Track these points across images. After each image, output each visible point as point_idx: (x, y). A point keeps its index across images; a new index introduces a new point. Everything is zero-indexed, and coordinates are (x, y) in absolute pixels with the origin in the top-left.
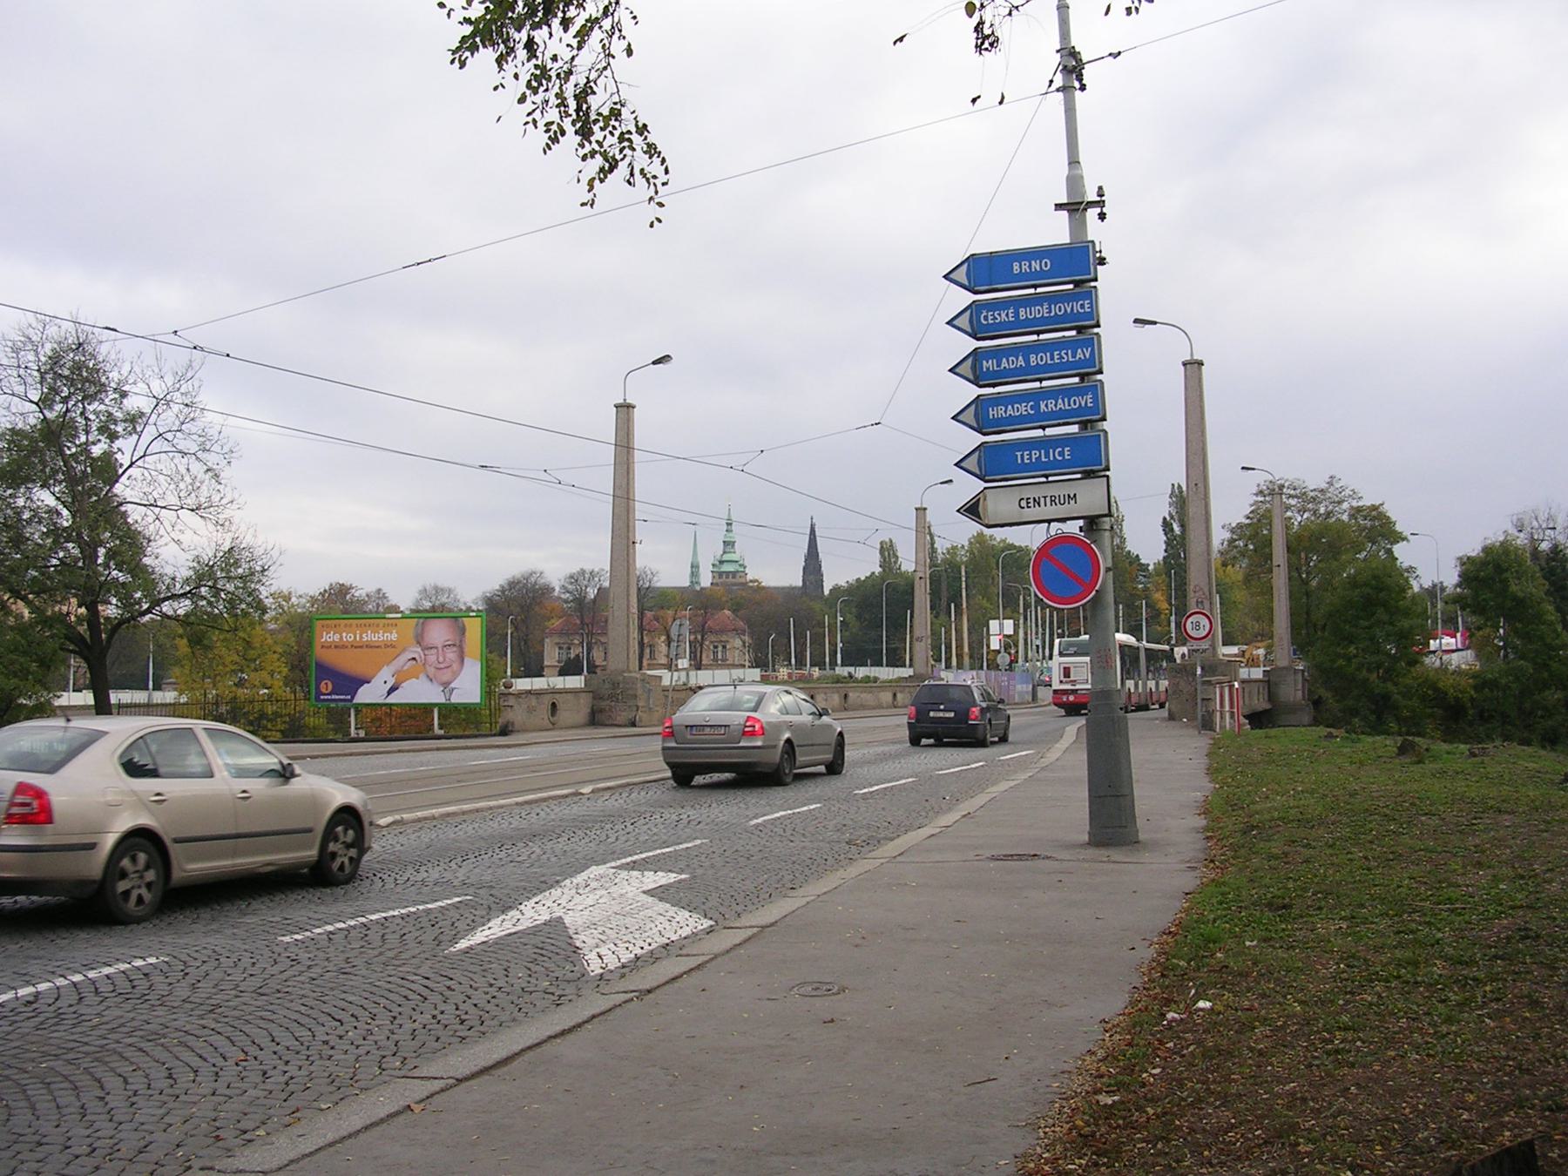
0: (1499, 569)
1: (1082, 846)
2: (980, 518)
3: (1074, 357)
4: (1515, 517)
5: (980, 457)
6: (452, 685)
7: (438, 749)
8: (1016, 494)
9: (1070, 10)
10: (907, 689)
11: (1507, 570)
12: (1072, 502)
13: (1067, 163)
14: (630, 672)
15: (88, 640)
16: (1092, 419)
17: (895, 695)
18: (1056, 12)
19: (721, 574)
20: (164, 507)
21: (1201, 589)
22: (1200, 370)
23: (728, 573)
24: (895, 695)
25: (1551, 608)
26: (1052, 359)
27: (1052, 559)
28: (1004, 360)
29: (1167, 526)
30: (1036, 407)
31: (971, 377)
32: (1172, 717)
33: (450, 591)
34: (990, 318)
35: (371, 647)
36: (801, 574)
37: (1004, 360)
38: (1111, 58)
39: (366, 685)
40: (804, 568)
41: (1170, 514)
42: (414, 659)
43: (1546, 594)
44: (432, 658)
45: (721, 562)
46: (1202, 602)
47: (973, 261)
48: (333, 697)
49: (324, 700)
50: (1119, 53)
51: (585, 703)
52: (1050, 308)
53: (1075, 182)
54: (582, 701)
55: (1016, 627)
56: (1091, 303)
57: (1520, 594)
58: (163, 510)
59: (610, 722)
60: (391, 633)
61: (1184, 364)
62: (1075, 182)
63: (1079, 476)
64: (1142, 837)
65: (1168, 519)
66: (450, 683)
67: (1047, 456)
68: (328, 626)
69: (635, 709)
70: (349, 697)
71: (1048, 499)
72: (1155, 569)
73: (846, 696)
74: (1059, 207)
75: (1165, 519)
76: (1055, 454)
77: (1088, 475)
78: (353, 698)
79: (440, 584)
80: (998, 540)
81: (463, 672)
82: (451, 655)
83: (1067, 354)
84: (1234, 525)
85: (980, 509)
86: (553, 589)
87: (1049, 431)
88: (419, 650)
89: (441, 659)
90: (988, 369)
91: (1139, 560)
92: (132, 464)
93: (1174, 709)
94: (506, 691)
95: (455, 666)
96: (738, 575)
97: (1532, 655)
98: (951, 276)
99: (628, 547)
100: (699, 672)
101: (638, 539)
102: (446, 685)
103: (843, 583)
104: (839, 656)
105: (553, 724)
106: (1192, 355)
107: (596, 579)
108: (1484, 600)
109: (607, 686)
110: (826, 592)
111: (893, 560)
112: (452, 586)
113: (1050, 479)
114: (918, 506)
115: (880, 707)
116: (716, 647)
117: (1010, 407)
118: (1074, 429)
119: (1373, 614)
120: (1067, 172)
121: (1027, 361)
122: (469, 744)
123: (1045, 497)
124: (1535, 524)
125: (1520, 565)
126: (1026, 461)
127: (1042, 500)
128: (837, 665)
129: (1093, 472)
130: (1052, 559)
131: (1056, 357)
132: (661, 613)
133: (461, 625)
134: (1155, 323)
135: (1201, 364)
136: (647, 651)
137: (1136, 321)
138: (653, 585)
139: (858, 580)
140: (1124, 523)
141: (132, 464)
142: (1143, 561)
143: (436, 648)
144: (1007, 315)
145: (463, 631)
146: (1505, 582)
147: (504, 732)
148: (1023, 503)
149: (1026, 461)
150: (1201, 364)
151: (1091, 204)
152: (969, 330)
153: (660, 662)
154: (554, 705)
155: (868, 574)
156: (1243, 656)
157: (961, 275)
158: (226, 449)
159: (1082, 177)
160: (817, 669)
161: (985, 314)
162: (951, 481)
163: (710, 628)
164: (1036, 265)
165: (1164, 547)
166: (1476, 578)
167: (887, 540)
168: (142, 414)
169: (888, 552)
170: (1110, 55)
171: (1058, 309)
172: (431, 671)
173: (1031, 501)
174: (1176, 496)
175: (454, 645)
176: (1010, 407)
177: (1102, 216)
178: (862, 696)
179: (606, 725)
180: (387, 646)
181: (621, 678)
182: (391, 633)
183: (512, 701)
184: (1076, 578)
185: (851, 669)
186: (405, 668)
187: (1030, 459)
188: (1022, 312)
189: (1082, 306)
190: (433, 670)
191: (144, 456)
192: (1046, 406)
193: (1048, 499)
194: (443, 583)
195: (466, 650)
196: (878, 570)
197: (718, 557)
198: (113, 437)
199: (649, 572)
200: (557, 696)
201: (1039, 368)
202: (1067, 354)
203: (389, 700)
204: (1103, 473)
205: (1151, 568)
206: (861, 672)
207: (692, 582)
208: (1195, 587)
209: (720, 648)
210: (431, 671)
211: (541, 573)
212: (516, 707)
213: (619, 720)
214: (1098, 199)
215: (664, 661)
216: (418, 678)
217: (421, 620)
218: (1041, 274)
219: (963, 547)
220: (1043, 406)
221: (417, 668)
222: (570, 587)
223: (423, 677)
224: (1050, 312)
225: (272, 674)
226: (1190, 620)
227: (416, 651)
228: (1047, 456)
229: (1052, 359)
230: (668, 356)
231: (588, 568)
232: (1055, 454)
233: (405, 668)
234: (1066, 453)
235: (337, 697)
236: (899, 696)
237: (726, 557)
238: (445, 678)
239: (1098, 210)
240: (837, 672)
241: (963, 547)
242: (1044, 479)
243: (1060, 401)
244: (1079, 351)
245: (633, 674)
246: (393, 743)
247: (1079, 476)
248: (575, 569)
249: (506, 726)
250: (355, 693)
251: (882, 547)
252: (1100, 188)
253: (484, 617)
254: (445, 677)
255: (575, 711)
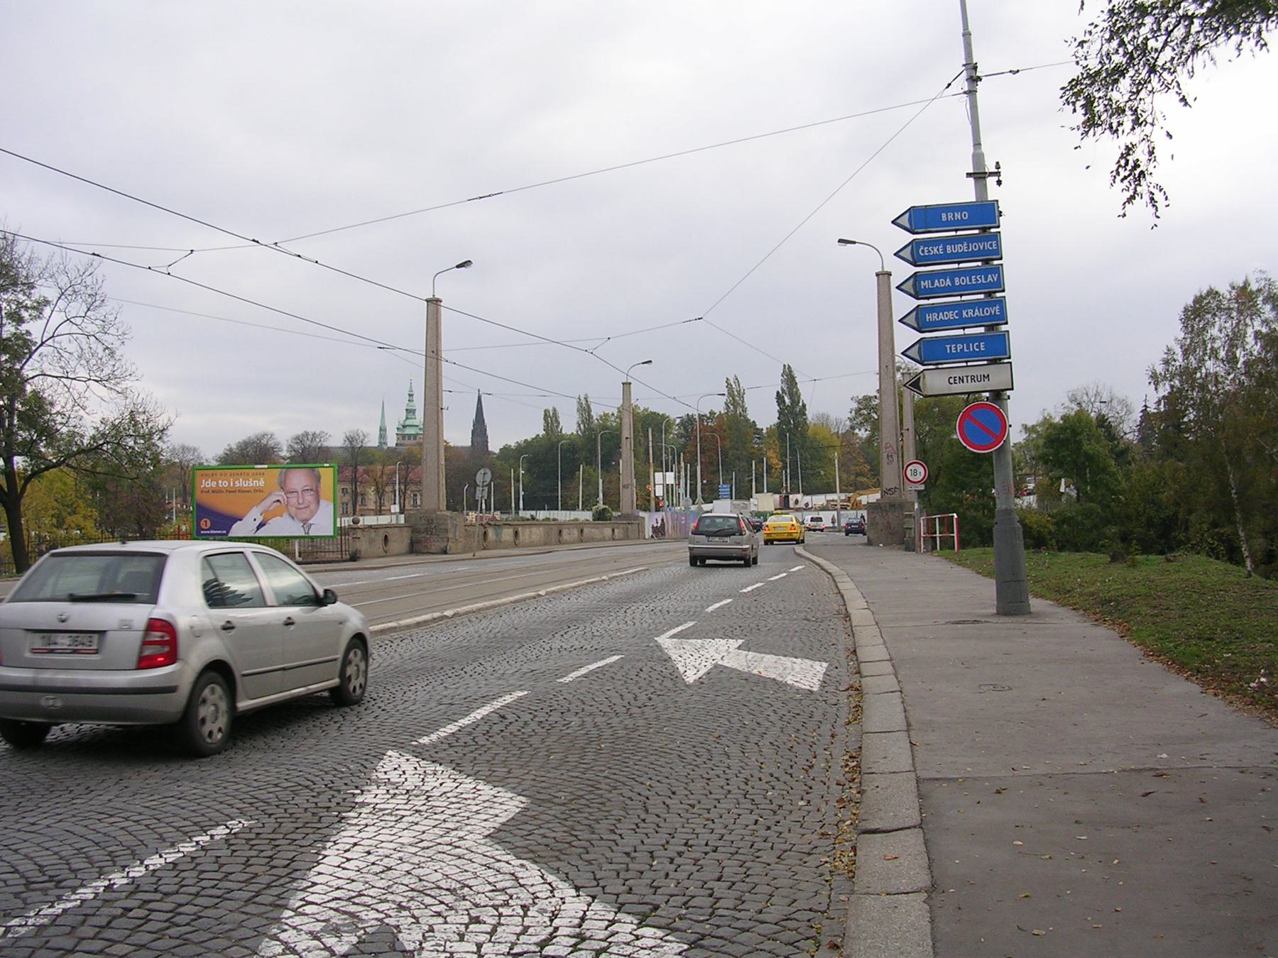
0: (1075, 433)
1: (993, 615)
2: (920, 390)
3: (986, 279)
4: (1071, 393)
5: (920, 348)
6: (310, 522)
7: (326, 571)
8: (946, 375)
9: (972, 37)
10: (621, 526)
11: (1080, 434)
12: (986, 380)
13: (972, 144)
14: (441, 511)
15: (6, 490)
16: (996, 319)
17: (613, 530)
18: (962, 38)
19: (404, 436)
20: (74, 379)
21: (891, 446)
22: (889, 279)
23: (410, 436)
24: (613, 530)
25: (1113, 463)
26: (971, 281)
27: (972, 419)
28: (936, 281)
29: (780, 398)
30: (960, 314)
31: (913, 292)
32: (870, 543)
33: (195, 450)
34: (926, 251)
35: (243, 492)
36: (471, 436)
37: (936, 281)
38: (1011, 74)
39: (239, 522)
40: (473, 432)
41: (782, 389)
42: (278, 501)
43: (1109, 452)
44: (293, 500)
45: (404, 426)
46: (891, 456)
47: (912, 211)
48: (212, 532)
49: (204, 534)
50: (1018, 71)
51: (406, 535)
52: (968, 246)
53: (978, 158)
54: (404, 534)
55: (678, 478)
56: (997, 243)
57: (1091, 452)
58: (74, 381)
59: (426, 550)
60: (259, 480)
61: (877, 275)
62: (978, 158)
63: (985, 362)
64: (1032, 609)
65: (781, 392)
66: (307, 520)
67: (968, 348)
68: (206, 475)
69: (446, 540)
70: (225, 532)
71: (969, 378)
72: (767, 432)
73: (582, 531)
74: (969, 175)
75: (778, 393)
76: (974, 347)
77: (993, 362)
78: (228, 532)
79: (186, 445)
80: (642, 409)
81: (319, 511)
82: (309, 497)
83: (981, 278)
84: (860, 397)
85: (921, 384)
86: (281, 450)
87: (968, 331)
88: (283, 493)
89: (301, 501)
90: (925, 287)
91: (755, 425)
92: (43, 343)
93: (871, 537)
94: (355, 526)
95: (313, 506)
96: (418, 437)
97: (1100, 498)
98: (898, 221)
99: (438, 412)
100: (379, 517)
101: (444, 406)
102: (305, 521)
103: (513, 444)
104: (521, 502)
105: (386, 552)
106: (883, 267)
107: (318, 440)
108: (1063, 456)
109: (423, 522)
110: (1016, 436)
111: (555, 424)
112: (195, 446)
113: (969, 364)
114: (625, 381)
115: (604, 539)
116: (415, 495)
117: (941, 314)
118: (982, 330)
119: (980, 466)
120: (972, 152)
121: (953, 282)
122: (347, 567)
123: (967, 377)
124: (1085, 398)
125: (1090, 431)
126: (953, 351)
127: (965, 378)
128: (519, 509)
129: (1000, 359)
130: (972, 419)
131: (973, 280)
132: (371, 467)
133: (316, 473)
134: (854, 243)
135: (890, 274)
136: (359, 499)
137: (840, 241)
138: (364, 445)
139: (526, 440)
140: (745, 396)
141: (43, 343)
142: (758, 427)
143: (297, 492)
144: (938, 250)
145: (318, 478)
146: (1079, 443)
147: (354, 558)
148: (952, 381)
149: (953, 351)
150: (890, 274)
151: (991, 174)
152: (910, 259)
153: (370, 507)
154: (386, 537)
155: (534, 436)
156: (849, 501)
157: (905, 221)
158: (120, 332)
159: (983, 154)
160: (499, 513)
161: (922, 248)
162: (651, 361)
163: (411, 480)
164: (958, 216)
165: (777, 415)
166: (1057, 440)
167: (551, 409)
168: (47, 302)
169: (551, 419)
170: (1011, 71)
171: (973, 247)
172: (293, 510)
173: (957, 379)
174: (787, 375)
175: (311, 490)
176: (941, 314)
177: (999, 183)
178: (593, 530)
179: (424, 553)
180: (256, 491)
181: (434, 516)
182: (259, 480)
183: (359, 534)
184: (989, 432)
185: (533, 513)
186: (271, 508)
187: (956, 349)
188: (948, 248)
189: (991, 245)
190: (294, 509)
191: (53, 336)
192: (967, 313)
193: (969, 378)
194: (190, 443)
195: (322, 495)
196: (542, 433)
197: (402, 423)
198: (20, 320)
199: (361, 434)
200: (388, 530)
201: (961, 288)
202: (981, 278)
203: (257, 535)
204: (1006, 361)
205: (764, 431)
206: (541, 515)
207: (380, 443)
208: (886, 444)
209: (419, 497)
210: (293, 510)
211: (272, 435)
212: (362, 538)
213: (433, 549)
214: (996, 170)
215: (372, 506)
216: (282, 516)
217: (284, 470)
218: (962, 222)
219: (613, 414)
220: (964, 314)
221: (281, 508)
222: (296, 446)
223: (285, 514)
224: (968, 248)
225: (85, 518)
226: (910, 468)
227: (280, 495)
228: (968, 348)
229: (971, 281)
230: (470, 261)
231: (311, 430)
232: (974, 347)
233: (271, 508)
234: (982, 346)
235: (215, 532)
236: (616, 531)
237: (409, 422)
238: (305, 516)
239: (996, 178)
240: (520, 515)
241: (613, 414)
242: (965, 364)
243: (977, 310)
244: (990, 276)
245: (444, 513)
246: (309, 566)
247: (985, 362)
248: (300, 432)
249: (356, 554)
250: (230, 528)
251: (545, 415)
252: (997, 163)
253: (337, 468)
254: (305, 515)
255: (400, 542)
